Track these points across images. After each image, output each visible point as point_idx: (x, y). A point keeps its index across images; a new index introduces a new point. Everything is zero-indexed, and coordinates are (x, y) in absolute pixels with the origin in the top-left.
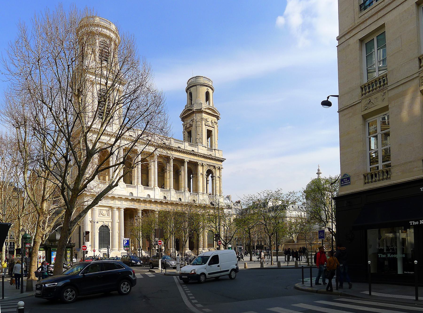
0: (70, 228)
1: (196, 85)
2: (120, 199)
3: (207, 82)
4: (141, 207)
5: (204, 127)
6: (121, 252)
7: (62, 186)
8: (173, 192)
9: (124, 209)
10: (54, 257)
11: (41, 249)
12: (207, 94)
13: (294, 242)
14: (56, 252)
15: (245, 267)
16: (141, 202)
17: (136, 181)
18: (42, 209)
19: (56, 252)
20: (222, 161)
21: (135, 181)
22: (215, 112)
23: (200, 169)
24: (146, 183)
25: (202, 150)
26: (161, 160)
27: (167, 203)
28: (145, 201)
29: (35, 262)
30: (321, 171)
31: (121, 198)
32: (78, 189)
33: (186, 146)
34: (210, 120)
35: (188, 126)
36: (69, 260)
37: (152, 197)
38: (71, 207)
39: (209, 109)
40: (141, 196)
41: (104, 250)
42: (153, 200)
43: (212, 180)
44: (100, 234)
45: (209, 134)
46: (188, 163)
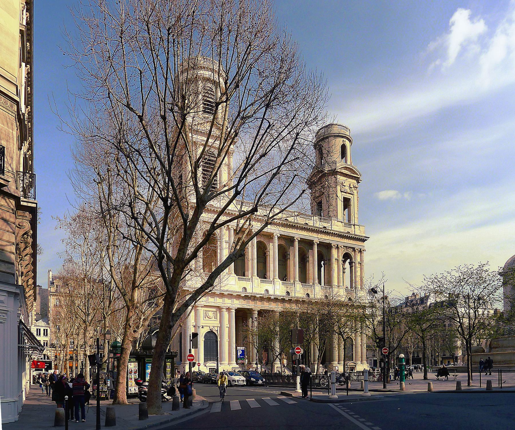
0: (171, 324)
1: (327, 138)
2: (230, 296)
3: (343, 131)
4: (257, 306)
5: (339, 194)
6: (231, 366)
7: (160, 253)
8: (299, 285)
9: (236, 310)
10: (148, 371)
11: (132, 360)
12: (344, 147)
13: (484, 351)
14: (151, 364)
15: (430, 390)
16: (257, 300)
17: (250, 272)
18: (132, 300)
19: (151, 364)
20: (364, 241)
21: (249, 273)
22: (354, 172)
23: (334, 252)
24: (263, 274)
25: (338, 227)
26: (283, 243)
27: (290, 301)
28: (262, 299)
29: (123, 377)
31: (231, 295)
32: (183, 260)
33: (316, 222)
34: (347, 184)
35: (317, 195)
36: (168, 376)
37: (271, 292)
38: (173, 289)
39: (346, 168)
40: (258, 292)
41: (212, 364)
42: (272, 297)
44: (205, 342)
45: (347, 203)
46: (318, 245)
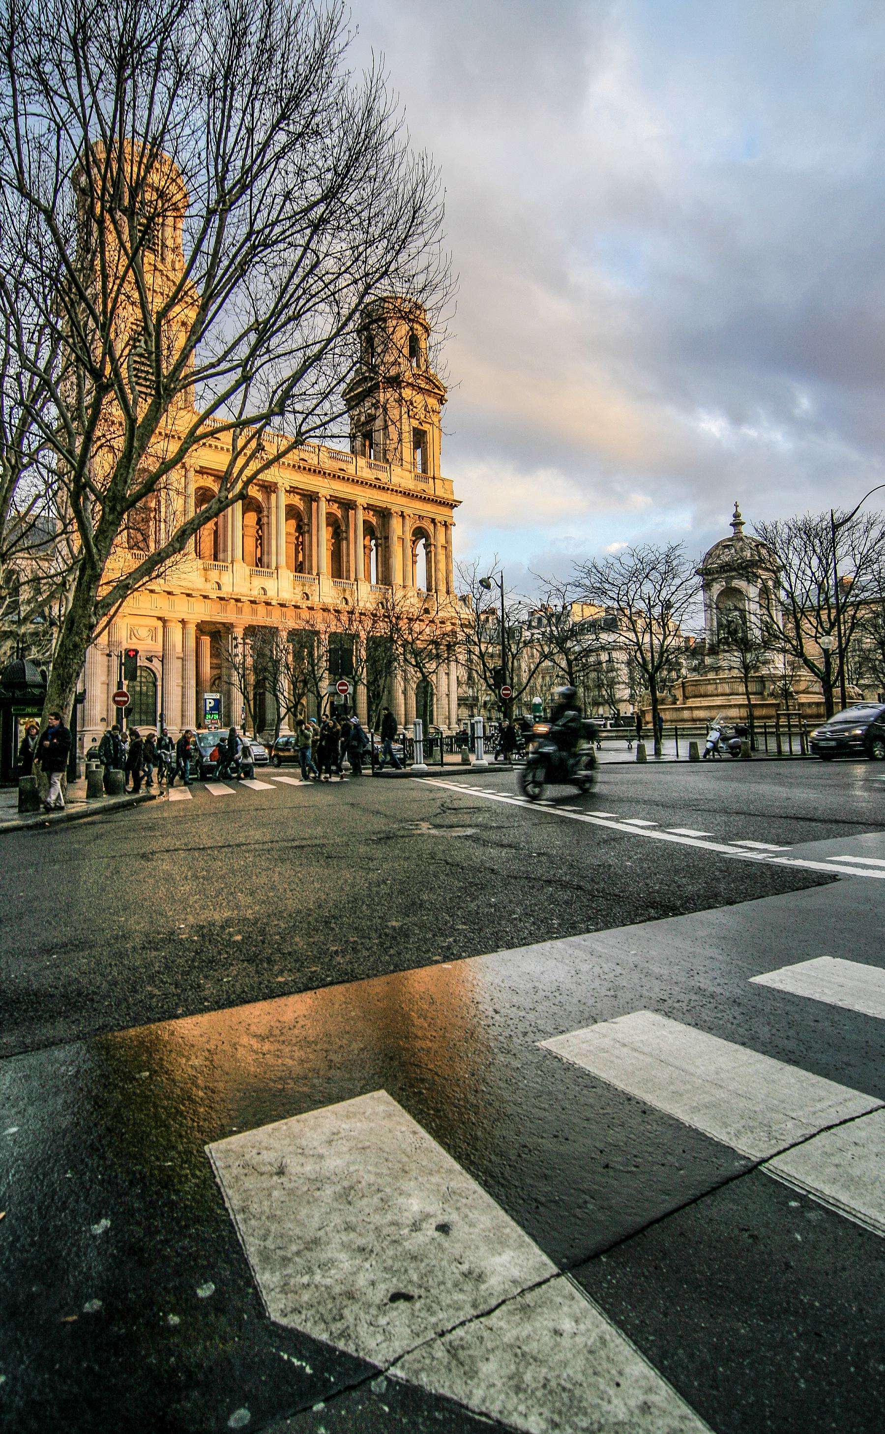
23: (396, 524)
25: (402, 477)
30: (742, 519)
33: (361, 467)
37: (271, 593)
43: (428, 553)
